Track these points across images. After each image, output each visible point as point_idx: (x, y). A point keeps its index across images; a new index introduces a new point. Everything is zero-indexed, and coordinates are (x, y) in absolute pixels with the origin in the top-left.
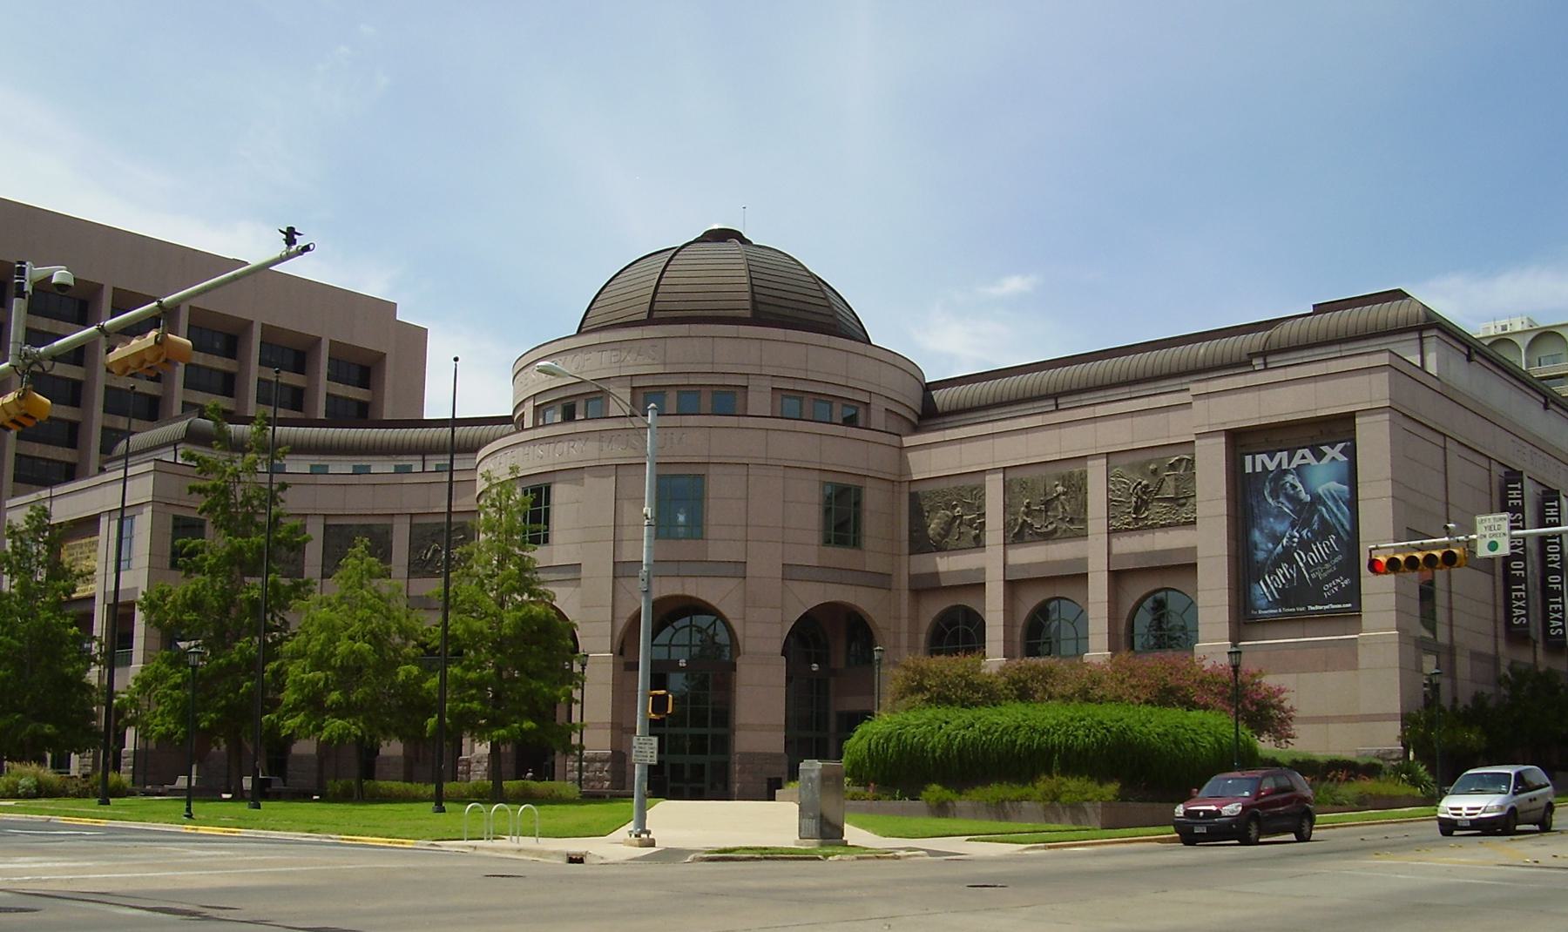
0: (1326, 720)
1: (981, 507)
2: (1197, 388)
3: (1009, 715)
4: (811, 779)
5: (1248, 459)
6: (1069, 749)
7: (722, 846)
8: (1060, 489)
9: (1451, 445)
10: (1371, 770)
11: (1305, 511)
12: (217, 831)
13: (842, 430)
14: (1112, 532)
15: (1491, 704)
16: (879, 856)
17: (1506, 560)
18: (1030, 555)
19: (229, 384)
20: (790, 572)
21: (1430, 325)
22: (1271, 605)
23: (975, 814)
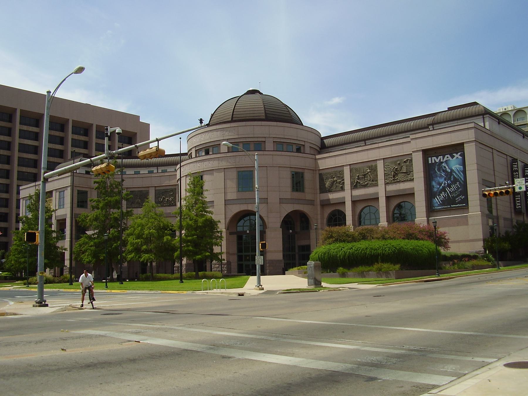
0: (458, 242)
1: (343, 177)
2: (412, 137)
3: (362, 245)
4: (311, 267)
5: (430, 159)
6: (383, 254)
7: (286, 289)
8: (368, 170)
9: (494, 151)
10: (475, 257)
11: (449, 175)
12: (119, 291)
13: (296, 154)
14: (386, 184)
15: (511, 234)
16: (335, 290)
17: (525, 192)
18: (359, 192)
19: (62, 141)
20: (282, 201)
21: (486, 113)
22: (439, 206)
23: (354, 276)
